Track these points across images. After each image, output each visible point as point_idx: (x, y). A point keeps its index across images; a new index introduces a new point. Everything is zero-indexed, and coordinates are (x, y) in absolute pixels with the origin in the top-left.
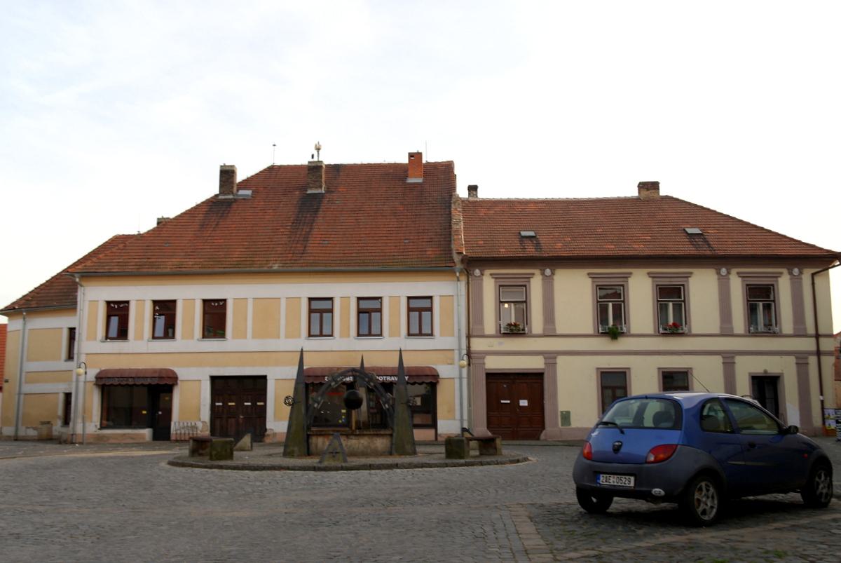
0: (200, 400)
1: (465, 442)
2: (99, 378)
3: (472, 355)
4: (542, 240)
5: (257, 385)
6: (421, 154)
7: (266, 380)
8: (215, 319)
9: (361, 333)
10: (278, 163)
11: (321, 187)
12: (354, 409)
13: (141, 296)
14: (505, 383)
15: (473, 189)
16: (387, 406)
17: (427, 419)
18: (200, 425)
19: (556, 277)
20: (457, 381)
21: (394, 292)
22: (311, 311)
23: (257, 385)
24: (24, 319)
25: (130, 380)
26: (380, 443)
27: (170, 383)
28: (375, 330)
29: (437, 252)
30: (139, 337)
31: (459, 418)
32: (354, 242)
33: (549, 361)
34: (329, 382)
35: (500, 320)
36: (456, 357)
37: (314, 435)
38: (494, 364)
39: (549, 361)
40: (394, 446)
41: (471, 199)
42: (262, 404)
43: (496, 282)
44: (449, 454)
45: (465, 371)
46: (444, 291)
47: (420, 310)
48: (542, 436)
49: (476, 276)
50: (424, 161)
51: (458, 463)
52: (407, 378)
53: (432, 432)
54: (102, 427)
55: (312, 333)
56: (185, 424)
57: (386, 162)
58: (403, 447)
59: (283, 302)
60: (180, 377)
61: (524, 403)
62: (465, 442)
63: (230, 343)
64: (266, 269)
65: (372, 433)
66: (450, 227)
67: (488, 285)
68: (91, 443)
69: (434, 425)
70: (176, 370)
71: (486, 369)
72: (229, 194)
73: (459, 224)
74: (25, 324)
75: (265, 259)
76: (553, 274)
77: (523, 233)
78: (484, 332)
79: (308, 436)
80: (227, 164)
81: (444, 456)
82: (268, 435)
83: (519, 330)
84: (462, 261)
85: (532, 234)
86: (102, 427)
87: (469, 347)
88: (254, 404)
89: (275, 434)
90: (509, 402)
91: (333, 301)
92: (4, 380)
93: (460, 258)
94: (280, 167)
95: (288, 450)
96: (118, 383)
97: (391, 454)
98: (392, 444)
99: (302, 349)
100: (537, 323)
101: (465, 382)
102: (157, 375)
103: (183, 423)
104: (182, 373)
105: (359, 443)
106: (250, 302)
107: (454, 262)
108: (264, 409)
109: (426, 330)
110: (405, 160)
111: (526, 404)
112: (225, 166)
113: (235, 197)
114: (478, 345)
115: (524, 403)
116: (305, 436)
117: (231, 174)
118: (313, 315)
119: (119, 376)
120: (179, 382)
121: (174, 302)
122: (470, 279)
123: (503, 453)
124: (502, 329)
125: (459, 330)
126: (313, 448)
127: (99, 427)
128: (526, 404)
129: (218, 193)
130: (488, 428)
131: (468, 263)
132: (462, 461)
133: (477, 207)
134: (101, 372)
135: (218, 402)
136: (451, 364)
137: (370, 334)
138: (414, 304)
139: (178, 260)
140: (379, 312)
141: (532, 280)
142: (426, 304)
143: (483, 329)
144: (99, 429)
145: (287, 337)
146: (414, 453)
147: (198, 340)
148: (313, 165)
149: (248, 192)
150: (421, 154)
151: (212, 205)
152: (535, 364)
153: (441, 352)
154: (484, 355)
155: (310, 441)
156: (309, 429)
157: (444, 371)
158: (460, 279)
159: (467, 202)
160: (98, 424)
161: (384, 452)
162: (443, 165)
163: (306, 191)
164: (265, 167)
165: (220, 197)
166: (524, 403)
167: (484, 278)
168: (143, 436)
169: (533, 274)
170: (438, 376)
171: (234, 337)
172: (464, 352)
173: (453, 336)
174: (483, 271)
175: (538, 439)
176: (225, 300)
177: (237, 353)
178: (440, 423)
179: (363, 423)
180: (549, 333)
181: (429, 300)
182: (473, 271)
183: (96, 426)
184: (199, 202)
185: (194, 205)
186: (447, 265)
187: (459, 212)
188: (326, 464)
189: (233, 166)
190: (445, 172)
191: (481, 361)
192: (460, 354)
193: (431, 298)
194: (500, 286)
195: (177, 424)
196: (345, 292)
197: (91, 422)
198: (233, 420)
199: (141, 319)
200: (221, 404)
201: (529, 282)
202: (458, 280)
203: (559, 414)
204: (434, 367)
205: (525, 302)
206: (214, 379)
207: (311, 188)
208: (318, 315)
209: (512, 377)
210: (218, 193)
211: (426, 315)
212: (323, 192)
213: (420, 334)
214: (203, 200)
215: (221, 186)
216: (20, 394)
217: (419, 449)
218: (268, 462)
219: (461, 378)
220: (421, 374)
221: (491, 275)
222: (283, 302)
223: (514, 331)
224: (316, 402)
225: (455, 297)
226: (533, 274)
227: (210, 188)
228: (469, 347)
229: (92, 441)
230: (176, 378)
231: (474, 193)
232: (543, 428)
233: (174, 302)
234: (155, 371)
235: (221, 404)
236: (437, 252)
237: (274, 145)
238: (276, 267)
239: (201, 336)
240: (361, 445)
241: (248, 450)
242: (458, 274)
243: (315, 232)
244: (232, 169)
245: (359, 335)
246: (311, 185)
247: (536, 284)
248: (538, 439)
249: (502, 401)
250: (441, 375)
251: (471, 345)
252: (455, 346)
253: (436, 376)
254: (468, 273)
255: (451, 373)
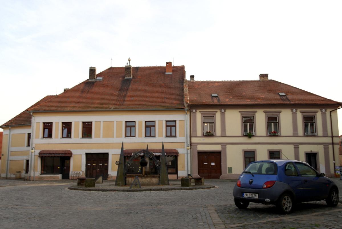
0: (81, 163)
1: (189, 180)
2: (40, 154)
3: (192, 145)
4: (221, 98)
5: (104, 157)
6: (171, 62)
7: (108, 154)
8: (87, 130)
9: (147, 135)
10: (113, 66)
11: (130, 76)
12: (144, 166)
13: (57, 120)
14: (205, 156)
15: (192, 77)
16: (157, 165)
17: (174, 170)
18: (81, 173)
19: (226, 113)
20: (186, 155)
21: (160, 119)
22: (126, 127)
23: (104, 157)
24: (10, 130)
25: (53, 154)
26: (155, 180)
27: (69, 156)
28: (152, 134)
29: (178, 103)
30: (57, 137)
31: (187, 170)
32: (144, 98)
33: (223, 147)
34: (134, 155)
35: (203, 130)
36: (186, 145)
37: (128, 177)
38: (201, 148)
39: (223, 147)
40: (160, 182)
41: (192, 81)
42: (107, 164)
43: (202, 115)
44: (183, 185)
45: (189, 151)
46: (180, 118)
47: (171, 126)
48: (221, 177)
49: (194, 112)
50: (172, 66)
51: (186, 189)
52: (165, 154)
53: (176, 176)
54: (41, 174)
55: (127, 136)
56: (75, 172)
57: (157, 66)
58: (164, 182)
59: (115, 123)
60: (73, 154)
61: (213, 164)
62: (189, 180)
63: (94, 139)
64: (108, 109)
65: (151, 176)
66: (183, 92)
67: (199, 116)
68: (37, 180)
69: (176, 173)
70: (72, 150)
71: (198, 150)
72: (93, 79)
73: (187, 91)
74: (10, 132)
75: (108, 105)
76: (225, 111)
77: (213, 95)
78: (197, 135)
79: (125, 178)
80: (92, 67)
81: (180, 185)
82: (109, 177)
83: (211, 134)
84: (188, 106)
85: (216, 95)
86: (41, 174)
87: (191, 141)
88: (103, 164)
89: (112, 177)
90: (207, 163)
91: (135, 122)
92: (1, 155)
93: (187, 105)
94: (114, 68)
95: (117, 183)
96: (48, 156)
97: (159, 185)
98: (159, 181)
99: (123, 142)
100: (218, 132)
101: (189, 155)
102: (64, 153)
103: (75, 172)
104: (74, 152)
105: (146, 180)
106: (102, 123)
107: (185, 107)
108: (107, 166)
109: (173, 134)
110: (165, 65)
111: (214, 164)
112: (91, 67)
113: (96, 80)
114: (194, 140)
115: (213, 164)
116: (124, 177)
117: (94, 71)
118: (127, 128)
119: (48, 153)
120: (73, 155)
121: (71, 123)
122: (191, 114)
123: (205, 184)
124: (204, 134)
125: (187, 134)
126: (127, 182)
127: (40, 174)
128: (214, 164)
129: (89, 78)
130: (198, 174)
131: (190, 107)
132: (188, 188)
133: (194, 84)
134: (41, 151)
135: (89, 164)
136: (183, 148)
137: (150, 136)
138: (168, 124)
139: (73, 106)
140: (154, 127)
141: (216, 114)
142: (173, 123)
143: (196, 134)
144: (40, 175)
145: (117, 137)
146: (169, 184)
147: (81, 138)
148: (127, 67)
149: (101, 78)
150: (171, 62)
151: (86, 83)
152: (218, 148)
153: (179, 143)
154: (197, 144)
155: (126, 179)
156: (125, 174)
157: (180, 151)
158: (187, 113)
159: (190, 82)
160: (40, 172)
161: (156, 184)
162: (180, 67)
163: (125, 78)
164: (108, 68)
165: (90, 80)
166: (213, 164)
167: (197, 113)
168: (58, 177)
169: (217, 111)
170: (178, 153)
171: (95, 137)
172: (189, 143)
173: (184, 136)
174: (197, 110)
175: (219, 179)
176: (91, 122)
177: (96, 144)
178: (179, 172)
179: (148, 172)
180: (223, 135)
181: (175, 122)
182: (193, 110)
183: (39, 173)
184: (81, 82)
185: (79, 83)
186: (182, 108)
187: (187, 86)
188: (132, 189)
189: (95, 68)
190: (181, 70)
191: (196, 147)
192: (187, 144)
193: (175, 121)
194: (203, 116)
195: (72, 172)
196: (140, 119)
197: (37, 172)
198: (95, 171)
199: (57, 130)
200: (90, 164)
201: (215, 115)
202: (186, 114)
203: (227, 168)
204: (177, 149)
205: (214, 123)
206: (87, 154)
207: (126, 76)
208: (129, 128)
209: (208, 153)
210: (89, 78)
211: (173, 128)
212: (132, 78)
213: (171, 136)
214: (83, 81)
215: (90, 76)
216: (8, 160)
217: (170, 183)
218: (109, 188)
219: (187, 154)
220: (171, 152)
221: (200, 112)
222: (115, 123)
223: (209, 135)
224: (129, 164)
225: (185, 121)
226: (217, 111)
227: (86, 76)
228: (191, 141)
229: (37, 179)
230: (72, 154)
231: (193, 78)
232: (221, 174)
233: (71, 123)
234: (63, 151)
235: (90, 164)
236: (178, 103)
237: (112, 59)
238: (112, 109)
239: (82, 137)
240: (147, 181)
241: (101, 183)
242: (186, 112)
243: (128, 94)
244: (94, 69)
245: (146, 136)
246: (126, 75)
247: (218, 116)
248: (219, 179)
249: (204, 163)
250: (180, 153)
251: (192, 140)
252: (185, 141)
253: (177, 153)
254: (190, 111)
255: (183, 152)
